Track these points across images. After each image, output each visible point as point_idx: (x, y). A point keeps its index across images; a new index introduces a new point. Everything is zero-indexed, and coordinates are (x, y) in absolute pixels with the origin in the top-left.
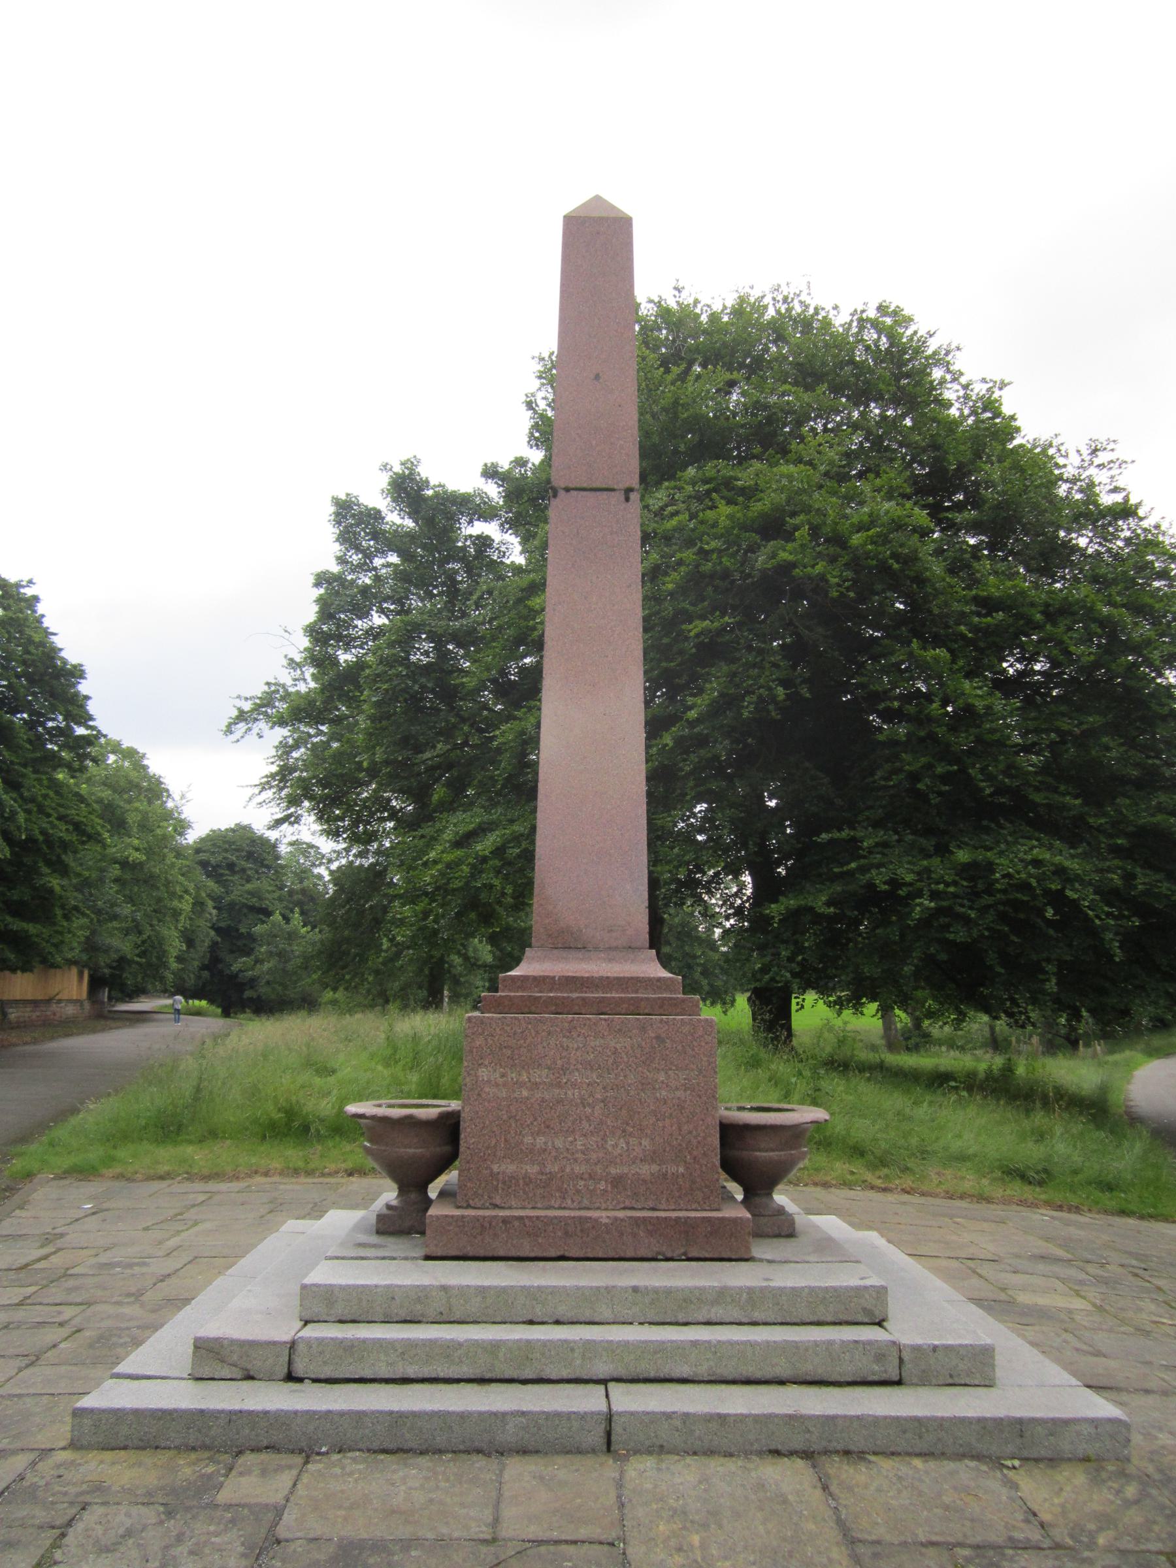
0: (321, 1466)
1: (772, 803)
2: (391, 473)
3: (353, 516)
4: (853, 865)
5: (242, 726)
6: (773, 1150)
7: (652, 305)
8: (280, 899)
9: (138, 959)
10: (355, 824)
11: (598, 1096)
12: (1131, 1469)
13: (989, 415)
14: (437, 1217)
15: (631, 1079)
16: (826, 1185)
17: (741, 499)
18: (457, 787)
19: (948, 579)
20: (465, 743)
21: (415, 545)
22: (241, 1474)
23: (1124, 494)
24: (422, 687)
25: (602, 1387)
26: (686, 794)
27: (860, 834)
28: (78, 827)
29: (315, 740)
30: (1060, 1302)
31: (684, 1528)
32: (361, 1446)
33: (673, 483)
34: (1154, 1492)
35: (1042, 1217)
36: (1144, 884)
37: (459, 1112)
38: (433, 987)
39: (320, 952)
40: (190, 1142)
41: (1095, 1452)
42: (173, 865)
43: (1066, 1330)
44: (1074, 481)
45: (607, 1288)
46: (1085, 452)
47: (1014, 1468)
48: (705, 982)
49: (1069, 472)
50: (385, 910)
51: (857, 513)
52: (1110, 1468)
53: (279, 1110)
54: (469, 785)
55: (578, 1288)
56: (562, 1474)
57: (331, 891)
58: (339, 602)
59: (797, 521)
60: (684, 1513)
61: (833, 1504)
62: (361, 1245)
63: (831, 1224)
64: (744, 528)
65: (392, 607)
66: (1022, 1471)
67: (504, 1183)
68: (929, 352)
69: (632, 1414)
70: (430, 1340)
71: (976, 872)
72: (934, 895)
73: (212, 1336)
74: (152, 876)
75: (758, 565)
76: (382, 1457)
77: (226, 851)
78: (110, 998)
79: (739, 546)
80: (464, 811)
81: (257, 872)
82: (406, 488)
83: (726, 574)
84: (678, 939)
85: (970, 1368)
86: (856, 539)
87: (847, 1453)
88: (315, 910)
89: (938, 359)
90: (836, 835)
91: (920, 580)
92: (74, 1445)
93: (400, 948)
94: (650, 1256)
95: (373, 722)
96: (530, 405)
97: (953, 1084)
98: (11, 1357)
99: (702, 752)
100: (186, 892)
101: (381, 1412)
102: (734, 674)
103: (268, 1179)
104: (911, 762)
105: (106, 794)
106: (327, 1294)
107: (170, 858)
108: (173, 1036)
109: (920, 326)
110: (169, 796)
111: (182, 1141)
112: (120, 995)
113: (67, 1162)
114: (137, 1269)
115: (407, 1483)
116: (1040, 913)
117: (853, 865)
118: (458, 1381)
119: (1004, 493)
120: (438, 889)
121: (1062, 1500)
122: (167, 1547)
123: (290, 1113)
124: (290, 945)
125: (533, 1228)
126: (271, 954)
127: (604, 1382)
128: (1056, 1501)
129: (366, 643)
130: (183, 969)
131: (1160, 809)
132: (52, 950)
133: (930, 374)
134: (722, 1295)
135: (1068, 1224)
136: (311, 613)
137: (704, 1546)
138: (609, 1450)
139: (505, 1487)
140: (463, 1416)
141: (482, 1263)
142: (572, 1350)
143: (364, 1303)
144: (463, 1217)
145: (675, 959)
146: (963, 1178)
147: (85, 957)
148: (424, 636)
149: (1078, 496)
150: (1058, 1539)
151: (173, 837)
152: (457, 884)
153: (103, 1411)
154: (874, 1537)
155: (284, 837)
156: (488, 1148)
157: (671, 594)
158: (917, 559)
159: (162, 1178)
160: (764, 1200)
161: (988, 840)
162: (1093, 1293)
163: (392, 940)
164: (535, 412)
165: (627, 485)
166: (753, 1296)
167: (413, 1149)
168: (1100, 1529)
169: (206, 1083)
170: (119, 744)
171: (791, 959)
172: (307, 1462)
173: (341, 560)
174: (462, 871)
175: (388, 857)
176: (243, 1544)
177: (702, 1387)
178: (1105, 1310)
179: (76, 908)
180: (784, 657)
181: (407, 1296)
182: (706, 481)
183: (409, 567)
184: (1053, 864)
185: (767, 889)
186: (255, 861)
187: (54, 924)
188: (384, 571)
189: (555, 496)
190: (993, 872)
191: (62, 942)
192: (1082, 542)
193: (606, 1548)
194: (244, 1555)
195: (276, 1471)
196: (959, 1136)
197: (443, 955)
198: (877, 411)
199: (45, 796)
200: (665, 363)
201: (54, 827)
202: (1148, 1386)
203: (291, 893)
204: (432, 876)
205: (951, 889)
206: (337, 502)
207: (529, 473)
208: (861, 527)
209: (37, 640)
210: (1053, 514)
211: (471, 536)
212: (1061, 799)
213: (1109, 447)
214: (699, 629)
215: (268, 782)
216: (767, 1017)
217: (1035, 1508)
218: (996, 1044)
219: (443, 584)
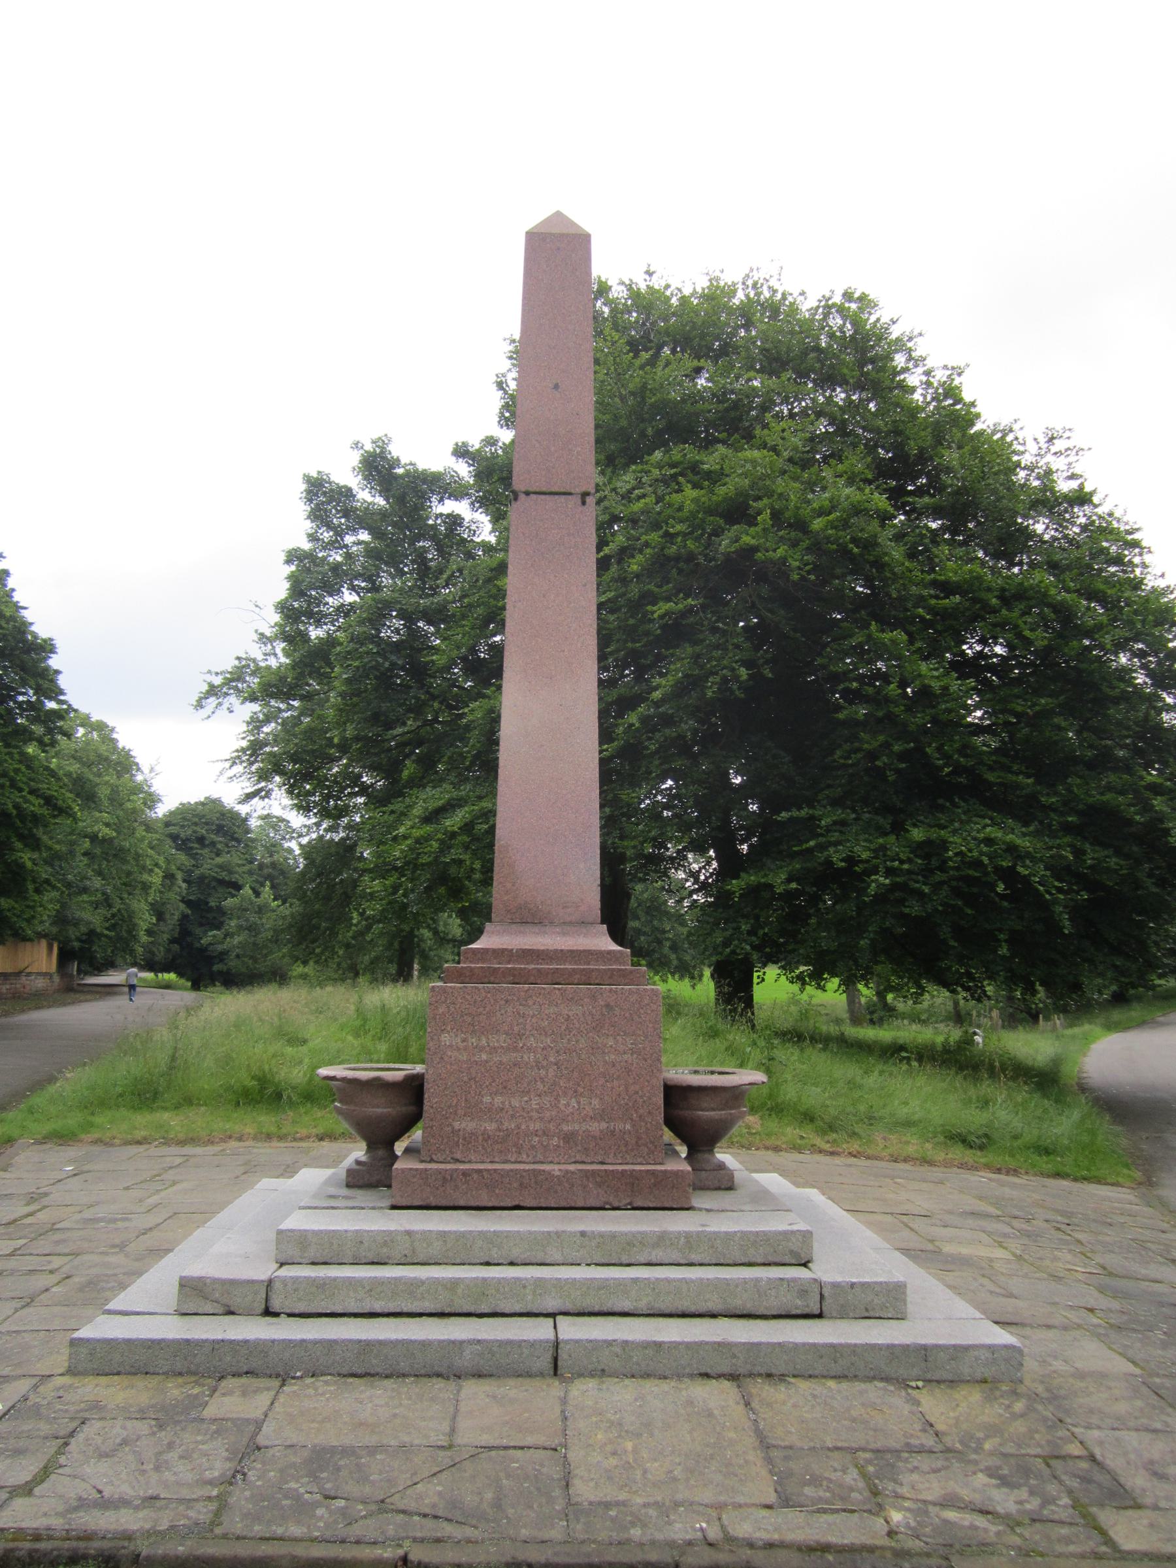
0: (295, 1388)
1: (738, 780)
2: (362, 452)
3: (325, 493)
4: (812, 843)
5: (213, 701)
6: (713, 1110)
7: (623, 288)
8: (250, 873)
9: (106, 932)
10: (326, 798)
11: (552, 1059)
12: (1021, 1389)
13: (950, 401)
14: (403, 1170)
15: (583, 1043)
16: (777, 1149)
17: (706, 483)
18: (427, 763)
19: (907, 564)
20: (435, 720)
21: (386, 523)
22: (224, 1395)
23: (1079, 482)
24: (393, 664)
25: (551, 1320)
26: (651, 773)
27: (818, 813)
28: (48, 801)
29: (286, 715)
30: (983, 1252)
31: (620, 1436)
32: (331, 1371)
33: (640, 467)
34: (1040, 1407)
35: (982, 1179)
36: (1093, 859)
37: (423, 1075)
38: (403, 960)
39: (291, 926)
40: (165, 1109)
41: (994, 1374)
42: (142, 839)
43: (983, 1276)
44: (1031, 468)
45: (557, 1233)
46: (1043, 440)
47: (918, 1388)
48: (673, 956)
49: (1026, 459)
50: (355, 883)
51: (820, 499)
52: (1004, 1388)
53: (253, 1078)
54: (439, 761)
55: (530, 1233)
56: (513, 1393)
57: (301, 866)
58: (310, 579)
59: (759, 504)
60: (620, 1424)
61: (753, 1417)
62: (331, 1197)
63: (771, 1181)
64: (710, 512)
65: (363, 584)
66: (924, 1391)
67: (464, 1139)
68: (893, 337)
69: (577, 1341)
70: (395, 1278)
71: (931, 850)
72: (889, 872)
73: (196, 1275)
74: (122, 850)
75: (722, 549)
76: (351, 1380)
77: (196, 824)
78: (79, 971)
79: (704, 529)
80: (434, 787)
81: (227, 846)
82: (377, 466)
83: (691, 557)
84: (647, 913)
85: (886, 1302)
86: (817, 524)
87: (769, 1376)
88: (286, 884)
89: (900, 345)
90: (795, 813)
91: (879, 565)
92: (71, 1372)
93: (371, 922)
94: (598, 1205)
95: (344, 698)
96: (500, 385)
97: (904, 1054)
98: (7, 1300)
99: (667, 731)
100: (156, 865)
101: (350, 1341)
102: (698, 656)
103: (242, 1144)
104: (869, 741)
105: (74, 768)
106: (301, 1239)
107: (140, 832)
108: (147, 1009)
109: (883, 314)
110: (139, 769)
111: (158, 1107)
112: (90, 969)
113: (49, 1127)
114: (120, 1224)
115: (374, 1401)
116: (993, 887)
117: (812, 843)
118: (420, 1315)
119: (963, 479)
120: (407, 863)
121: (957, 1414)
122: (160, 1453)
123: (263, 1081)
124: (260, 918)
125: (492, 1180)
126: (240, 928)
127: (553, 1315)
128: (952, 1414)
129: (337, 620)
130: (152, 943)
131: (1109, 788)
132: (24, 925)
133: (892, 360)
134: (662, 1239)
135: (1002, 1184)
136: (282, 590)
137: (635, 1451)
138: (555, 1374)
139: (462, 1404)
140: (425, 1344)
141: (442, 1212)
142: (524, 1287)
143: (335, 1246)
144: (426, 1170)
145: (645, 934)
146: (908, 1143)
147: (55, 930)
148: (394, 614)
149: (1036, 483)
150: (949, 1445)
151: (143, 811)
152: (425, 859)
153: (98, 1340)
154: (787, 1443)
155: (254, 811)
156: (449, 1107)
157: (637, 576)
158: (877, 544)
159: (139, 1143)
160: (706, 1156)
161: (943, 818)
162: (1015, 1246)
163: (362, 914)
164: (506, 392)
165: (584, 489)
166: (691, 1240)
167: (381, 1109)
168: (987, 1437)
169: (181, 1052)
170: (88, 717)
171: (749, 933)
172: (283, 1385)
173: (313, 538)
174: (431, 846)
175: (358, 831)
176: (227, 1450)
177: (641, 1319)
178: (1025, 1260)
179: (47, 881)
180: (747, 639)
181: (375, 1241)
182: (673, 465)
183: (376, 544)
184: (1004, 843)
185: (730, 865)
186: (225, 834)
187: (26, 898)
188: (355, 548)
189: (516, 499)
190: (947, 850)
191: (33, 917)
192: (1039, 528)
193: (549, 1452)
194: (228, 1459)
195: (255, 1392)
196: (906, 1103)
197: (412, 930)
198: (843, 395)
199: (17, 771)
200: (634, 347)
201: (27, 801)
202: (1050, 1322)
203: (261, 866)
204: (402, 851)
205: (906, 866)
206: (308, 479)
207: (500, 452)
208: (821, 513)
209: (8, 614)
210: (1010, 501)
211: (441, 515)
212: (1014, 778)
213: (1065, 435)
214: (662, 611)
215: (239, 757)
216: (726, 989)
217: (932, 1420)
218: (959, 1018)
219: (413, 562)
